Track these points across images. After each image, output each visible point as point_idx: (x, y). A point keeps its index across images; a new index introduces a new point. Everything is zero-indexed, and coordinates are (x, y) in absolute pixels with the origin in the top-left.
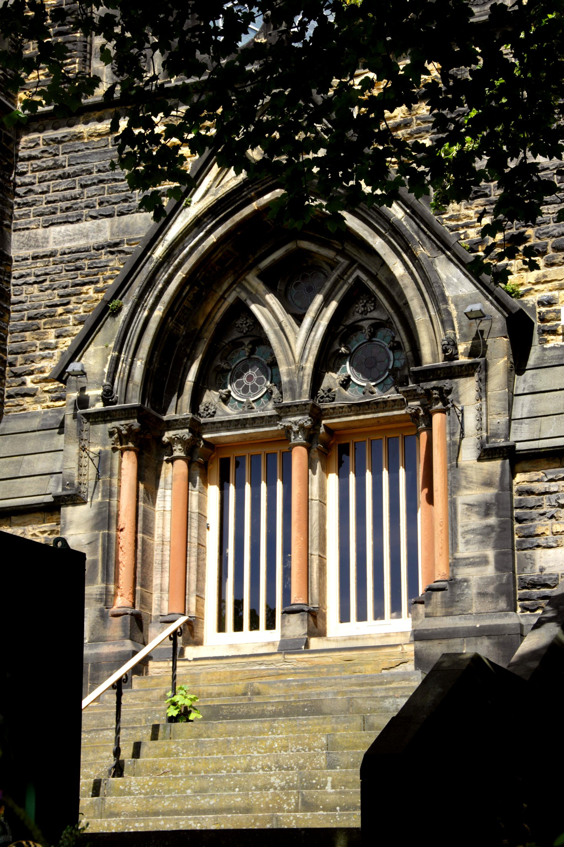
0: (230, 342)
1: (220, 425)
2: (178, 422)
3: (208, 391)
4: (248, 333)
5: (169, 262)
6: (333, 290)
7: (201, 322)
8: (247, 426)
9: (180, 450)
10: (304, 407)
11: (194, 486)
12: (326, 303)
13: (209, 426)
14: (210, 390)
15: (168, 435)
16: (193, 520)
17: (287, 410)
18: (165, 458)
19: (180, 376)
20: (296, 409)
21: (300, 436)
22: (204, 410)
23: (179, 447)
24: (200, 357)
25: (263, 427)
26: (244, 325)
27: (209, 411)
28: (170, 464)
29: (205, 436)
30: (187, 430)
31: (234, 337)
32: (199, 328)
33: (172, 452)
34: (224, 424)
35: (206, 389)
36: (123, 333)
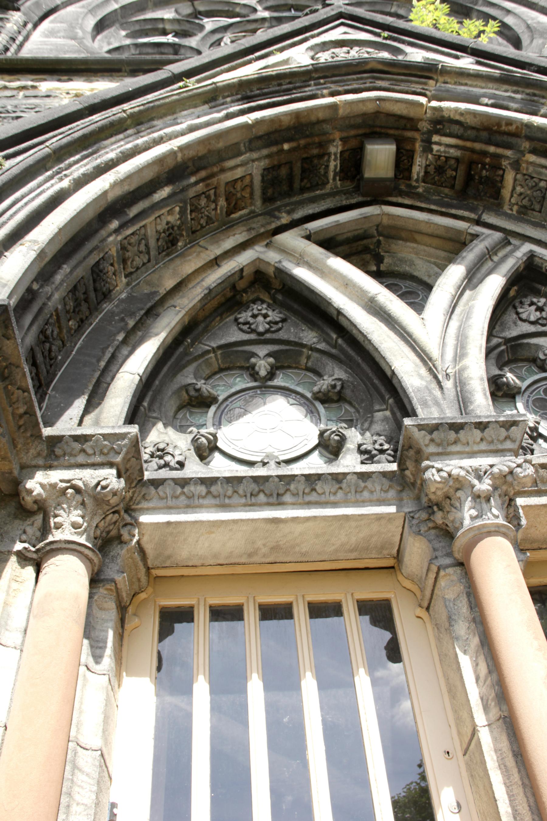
0: (220, 347)
1: (202, 489)
2: (87, 446)
3: (160, 425)
4: (268, 336)
5: (139, 132)
6: (478, 269)
7: (169, 284)
8: (287, 498)
9: (75, 526)
10: (503, 433)
11: (98, 658)
12: (472, 280)
13: (167, 489)
14: (165, 425)
15: (37, 483)
16: (80, 777)
17: (452, 435)
18: (19, 546)
19: (103, 364)
20: (477, 433)
21: (495, 511)
22: (152, 456)
23: (76, 516)
24: (163, 335)
25: (335, 504)
26: (260, 319)
27: (168, 458)
28: (30, 570)
29: (144, 519)
30: (114, 471)
31: (233, 339)
32: (162, 291)
33: (45, 530)
34: (216, 489)
35: (159, 419)
36: (50, 67)
